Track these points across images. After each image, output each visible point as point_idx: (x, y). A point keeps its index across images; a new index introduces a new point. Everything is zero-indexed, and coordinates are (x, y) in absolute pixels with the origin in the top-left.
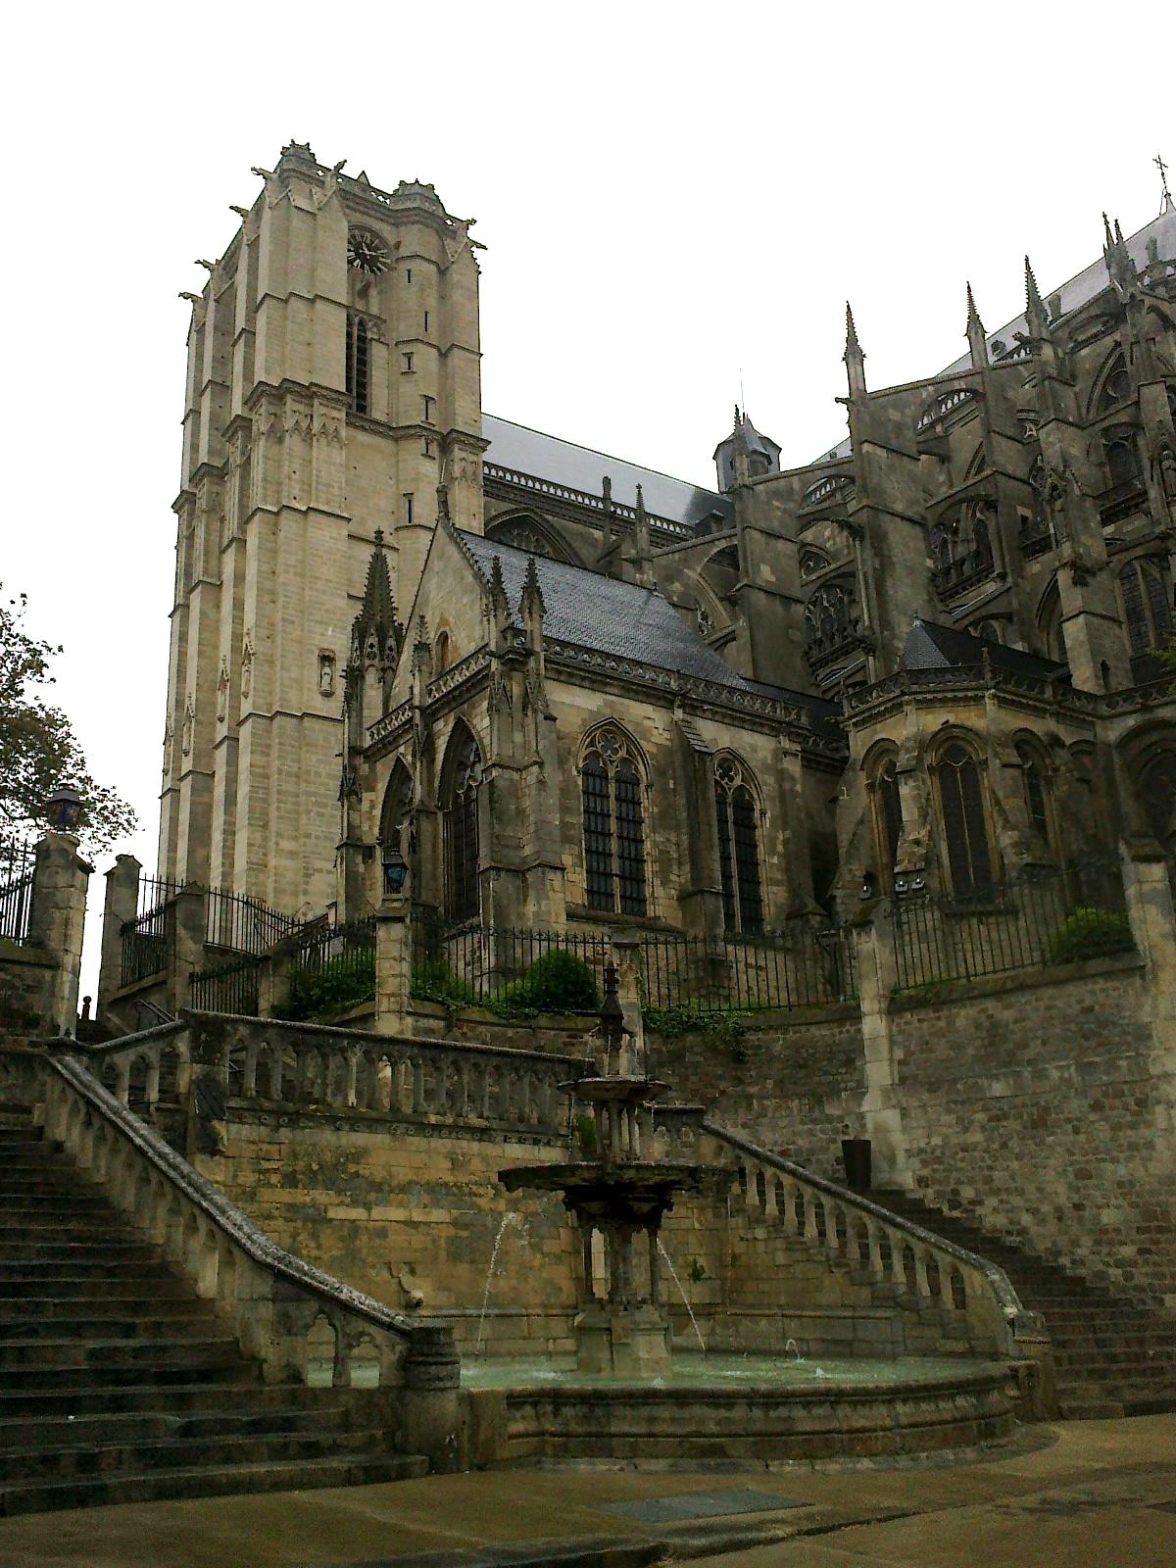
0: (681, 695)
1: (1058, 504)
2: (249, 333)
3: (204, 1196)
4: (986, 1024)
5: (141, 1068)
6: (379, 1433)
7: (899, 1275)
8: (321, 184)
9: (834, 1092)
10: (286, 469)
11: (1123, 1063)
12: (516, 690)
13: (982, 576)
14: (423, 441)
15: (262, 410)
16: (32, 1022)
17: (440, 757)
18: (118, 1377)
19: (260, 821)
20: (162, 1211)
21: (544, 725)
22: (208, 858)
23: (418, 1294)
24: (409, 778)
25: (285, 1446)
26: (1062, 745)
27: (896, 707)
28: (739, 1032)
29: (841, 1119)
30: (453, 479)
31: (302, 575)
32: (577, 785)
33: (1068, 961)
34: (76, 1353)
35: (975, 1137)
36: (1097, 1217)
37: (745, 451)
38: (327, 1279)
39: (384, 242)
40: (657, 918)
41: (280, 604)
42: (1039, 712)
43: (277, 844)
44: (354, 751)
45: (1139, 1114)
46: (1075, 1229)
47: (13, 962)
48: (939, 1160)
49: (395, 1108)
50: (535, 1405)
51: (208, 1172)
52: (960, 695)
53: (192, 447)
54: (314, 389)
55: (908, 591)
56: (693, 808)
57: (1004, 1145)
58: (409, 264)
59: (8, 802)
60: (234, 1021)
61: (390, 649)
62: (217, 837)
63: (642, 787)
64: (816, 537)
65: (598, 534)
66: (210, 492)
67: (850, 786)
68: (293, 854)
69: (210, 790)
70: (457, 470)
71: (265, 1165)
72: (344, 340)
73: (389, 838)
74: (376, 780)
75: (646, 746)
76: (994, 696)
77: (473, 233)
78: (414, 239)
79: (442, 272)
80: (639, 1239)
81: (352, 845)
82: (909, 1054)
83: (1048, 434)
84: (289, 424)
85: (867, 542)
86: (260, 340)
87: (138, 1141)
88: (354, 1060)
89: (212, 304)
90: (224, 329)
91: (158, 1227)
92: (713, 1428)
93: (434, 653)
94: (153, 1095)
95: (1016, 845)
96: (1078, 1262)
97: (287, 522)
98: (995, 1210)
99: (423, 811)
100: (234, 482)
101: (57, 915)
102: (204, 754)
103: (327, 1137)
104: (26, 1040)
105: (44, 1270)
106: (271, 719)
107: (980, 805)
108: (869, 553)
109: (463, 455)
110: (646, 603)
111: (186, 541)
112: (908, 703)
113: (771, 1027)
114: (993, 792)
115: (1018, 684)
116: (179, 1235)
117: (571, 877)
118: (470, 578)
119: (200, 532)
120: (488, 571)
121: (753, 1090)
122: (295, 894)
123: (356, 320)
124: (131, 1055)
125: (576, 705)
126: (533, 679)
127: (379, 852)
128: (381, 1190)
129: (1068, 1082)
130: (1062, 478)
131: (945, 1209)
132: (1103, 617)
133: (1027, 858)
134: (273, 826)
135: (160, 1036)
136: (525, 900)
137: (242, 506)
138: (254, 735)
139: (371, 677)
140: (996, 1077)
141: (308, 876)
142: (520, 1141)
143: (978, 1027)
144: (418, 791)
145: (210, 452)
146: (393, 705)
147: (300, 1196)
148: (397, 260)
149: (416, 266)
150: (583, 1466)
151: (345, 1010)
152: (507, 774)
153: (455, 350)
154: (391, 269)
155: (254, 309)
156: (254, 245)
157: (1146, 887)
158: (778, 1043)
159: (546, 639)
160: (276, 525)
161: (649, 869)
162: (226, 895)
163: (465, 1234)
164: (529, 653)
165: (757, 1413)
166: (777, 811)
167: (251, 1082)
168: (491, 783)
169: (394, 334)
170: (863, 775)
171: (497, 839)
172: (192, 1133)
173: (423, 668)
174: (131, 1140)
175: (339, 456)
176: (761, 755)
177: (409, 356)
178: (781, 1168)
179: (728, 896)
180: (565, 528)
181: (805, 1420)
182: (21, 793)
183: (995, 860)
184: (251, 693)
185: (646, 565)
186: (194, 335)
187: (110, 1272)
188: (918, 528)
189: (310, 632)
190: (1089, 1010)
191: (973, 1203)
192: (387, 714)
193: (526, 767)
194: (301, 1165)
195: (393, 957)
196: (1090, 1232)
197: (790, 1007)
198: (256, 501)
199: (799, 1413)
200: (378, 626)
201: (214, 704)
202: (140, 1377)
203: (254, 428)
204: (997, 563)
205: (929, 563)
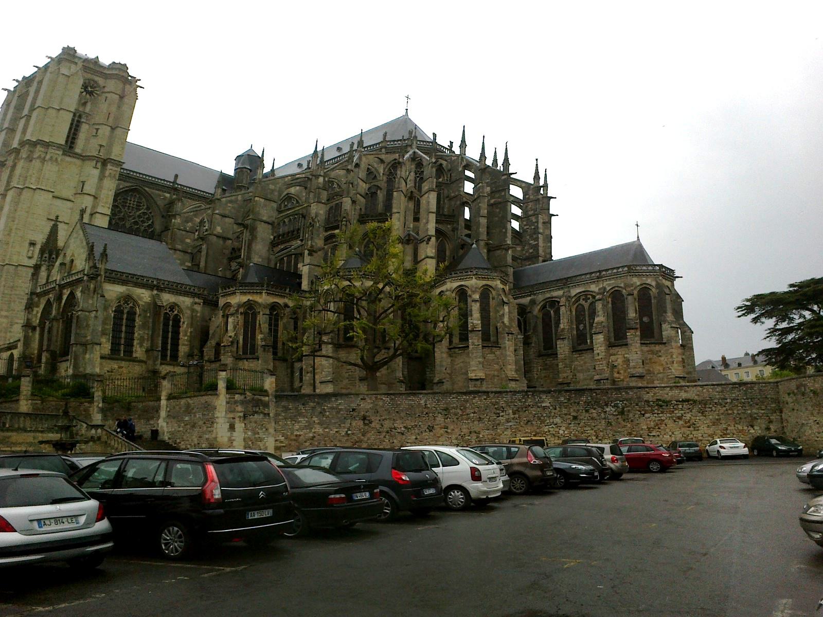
0: (158, 286)
2: (29, 117)
9: (152, 418)
12: (92, 286)
14: (95, 162)
17: (64, 301)
21: (100, 299)
26: (289, 307)
27: (234, 293)
28: (129, 403)
32: (111, 316)
35: (181, 429)
37: (250, 162)
40: (136, 357)
44: (32, 293)
56: (154, 323)
58: (107, 95)
61: (53, 258)
63: (137, 315)
74: (40, 304)
75: (140, 303)
76: (265, 293)
77: (138, 83)
82: (171, 409)
86: (32, 122)
89: (16, 98)
95: (261, 339)
97: (26, 194)
109: (111, 167)
114: (260, 321)
118: (85, 243)
125: (114, 291)
126: (99, 283)
129: (199, 417)
132: (316, 266)
133: (263, 343)
136: (86, 352)
139: (43, 268)
148: (103, 92)
152: (84, 313)
155: (32, 109)
156: (40, 82)
158: (140, 405)
160: (21, 193)
161: (135, 342)
168: (78, 317)
169: (93, 120)
173: (63, 271)
175: (55, 168)
176: (186, 304)
177: (97, 130)
180: (153, 193)
185: (177, 217)
186: (5, 106)
188: (270, 225)
190: (206, 402)
192: (47, 282)
198: (14, 183)
200: (50, 250)
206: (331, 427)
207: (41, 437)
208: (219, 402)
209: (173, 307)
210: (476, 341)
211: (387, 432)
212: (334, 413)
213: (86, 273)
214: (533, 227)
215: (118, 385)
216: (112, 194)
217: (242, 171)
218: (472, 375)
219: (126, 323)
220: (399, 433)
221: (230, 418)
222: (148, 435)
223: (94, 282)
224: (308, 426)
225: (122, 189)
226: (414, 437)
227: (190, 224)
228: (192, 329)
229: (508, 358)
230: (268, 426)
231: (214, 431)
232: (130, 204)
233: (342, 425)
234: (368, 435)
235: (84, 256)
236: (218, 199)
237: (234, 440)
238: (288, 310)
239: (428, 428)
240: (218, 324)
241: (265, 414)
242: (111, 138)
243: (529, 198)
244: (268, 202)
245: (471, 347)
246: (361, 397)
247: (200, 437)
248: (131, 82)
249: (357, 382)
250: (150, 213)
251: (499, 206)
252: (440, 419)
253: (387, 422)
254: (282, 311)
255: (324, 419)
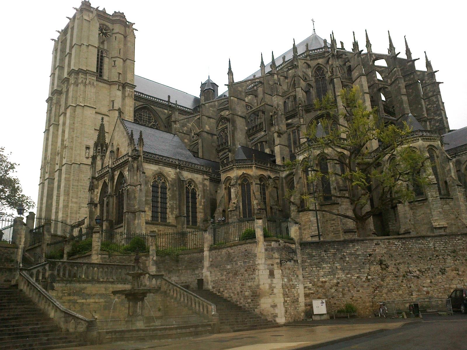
0: (179, 166)
1: (276, 116)
2: (70, 54)
3: (52, 299)
4: (228, 253)
5: (38, 272)
6: (82, 339)
7: (197, 307)
8: (92, 12)
10: (79, 94)
11: (251, 261)
12: (135, 165)
13: (261, 130)
14: (118, 86)
15: (72, 77)
16: (12, 261)
17: (115, 181)
18: (35, 332)
19: (67, 194)
20: (43, 302)
21: (142, 175)
22: (52, 203)
23: (96, 317)
24: (107, 186)
25: (65, 341)
26: (271, 178)
27: (232, 169)
28: (178, 255)
29: (198, 274)
30: (125, 97)
31: (82, 124)
33: (244, 240)
34: (28, 328)
35: (224, 277)
36: (244, 293)
37: (209, 89)
38: (74, 313)
39: (109, 29)
41: (75, 132)
42: (266, 170)
43: (71, 200)
44: (93, 178)
45: (253, 272)
46: (240, 296)
47: (8, 248)
48: (217, 283)
49: (93, 278)
50: (111, 333)
51: (52, 294)
52: (247, 166)
53: (52, 84)
54: (87, 71)
55: (241, 136)
56: (180, 195)
57: (229, 279)
58: (116, 35)
59: (3, 201)
60: (58, 261)
61: (104, 150)
62: (55, 198)
63: (167, 189)
64: (224, 114)
65: (166, 111)
66: (57, 98)
67: (220, 188)
68: (76, 203)
69: (53, 183)
70: (127, 94)
71: (64, 292)
72: (96, 60)
73: (101, 202)
76: (255, 167)
77: (134, 27)
78: (117, 28)
79: (125, 37)
80: (139, 304)
81: (91, 203)
82: (213, 259)
83: (274, 98)
84: (80, 81)
85: (231, 123)
87: (39, 289)
88: (84, 268)
89: (60, 43)
90: (63, 50)
91: (42, 305)
92: (143, 335)
93: (115, 153)
94: (41, 278)
95: (257, 204)
96: (241, 303)
97: (79, 110)
98: (226, 293)
99: (111, 196)
100: (64, 96)
101: (18, 236)
102: (52, 173)
103: (78, 285)
104: (10, 265)
105: (21, 315)
106: (71, 165)
107: (250, 194)
108: (231, 125)
110: (173, 138)
111: (49, 111)
112: (235, 168)
113: (185, 254)
114: (253, 190)
115: (261, 163)
116: (47, 307)
117: (148, 213)
118: (125, 134)
119: (54, 109)
120: (130, 132)
121: (180, 268)
122: (76, 214)
123: (100, 51)
124: (36, 270)
125: (151, 169)
126: (140, 163)
127: (98, 205)
128: (89, 296)
130: (277, 110)
131: (217, 293)
132: (284, 145)
133: (259, 207)
134: (71, 195)
135: (42, 265)
137: (66, 104)
138: (66, 169)
139: (99, 158)
140: (228, 264)
141: (80, 208)
142: (121, 284)
143: (226, 254)
144: (109, 190)
145: (58, 86)
146: (104, 166)
147: (71, 298)
148: (113, 34)
149: (117, 35)
150: (119, 343)
151: (85, 253)
153: (128, 60)
154: (111, 36)
155: (71, 47)
156: (73, 28)
157: (258, 225)
158: (186, 257)
159: (144, 152)
160: (75, 110)
162: (56, 221)
163: (107, 304)
164: (139, 156)
165: (151, 332)
166: (203, 194)
167: (61, 274)
168: (128, 190)
169: (110, 55)
170: (224, 185)
171: (128, 204)
172: (48, 286)
173: (112, 157)
174: (37, 289)
175: (93, 90)
177: (115, 61)
178: (177, 287)
179: (188, 216)
180: (157, 110)
181: (159, 333)
182: (6, 198)
183: (252, 207)
184: (66, 157)
185: (177, 122)
187: (33, 314)
188: (244, 119)
189: (83, 140)
190: (246, 250)
191: (223, 292)
192: (102, 168)
193: (137, 185)
194: (71, 291)
195: (97, 241)
196: (243, 297)
197: (190, 249)
198: (70, 103)
199: (159, 332)
200: (101, 145)
201: (55, 159)
202: (39, 332)
203: (70, 82)
204: (264, 127)
205: (246, 128)
206: (352, 272)
207: (112, 288)
208: (259, 250)
209: (191, 182)
210: (434, 193)
211: (404, 276)
212: (353, 259)
213: (130, 154)
214: (435, 105)
215: (163, 246)
216: (132, 109)
217: (208, 91)
218: (435, 224)
219: (161, 195)
220: (414, 276)
221: (269, 265)
222: (194, 284)
223: (136, 162)
224: (332, 271)
225: (138, 106)
226: (429, 281)
227: (185, 128)
228: (205, 200)
229: (462, 208)
230: (298, 272)
231: (256, 278)
232: (144, 118)
233: (362, 270)
234: (387, 280)
235: (126, 144)
236: (203, 104)
237: (275, 287)
238: (271, 181)
239: (440, 271)
240: (222, 195)
241: (295, 261)
242: (124, 68)
243: (425, 83)
244: (239, 101)
245: (430, 199)
246: (375, 242)
247: (243, 285)
248: (129, 26)
249: (341, 235)
250: (157, 125)
251: (411, 87)
252: (450, 260)
253: (401, 266)
254: (267, 182)
255: (345, 264)
